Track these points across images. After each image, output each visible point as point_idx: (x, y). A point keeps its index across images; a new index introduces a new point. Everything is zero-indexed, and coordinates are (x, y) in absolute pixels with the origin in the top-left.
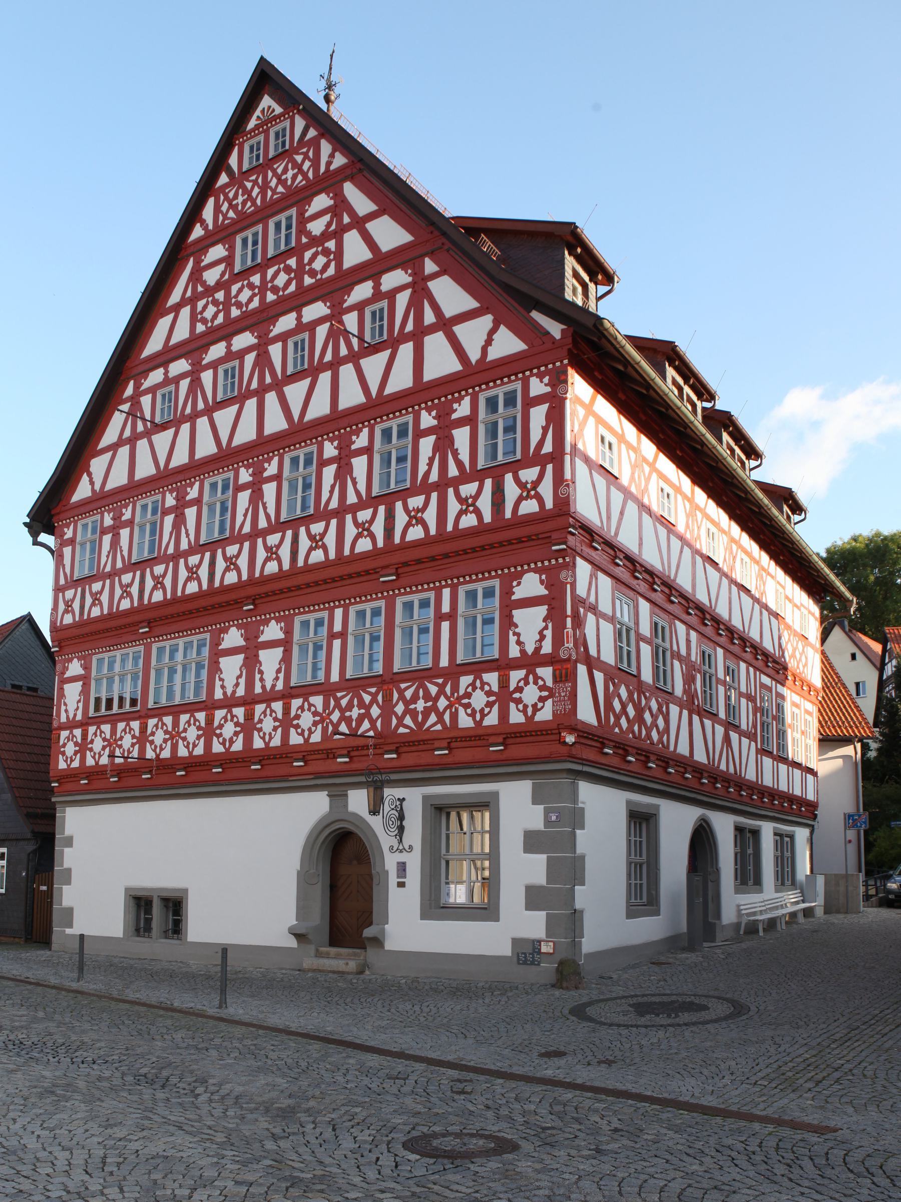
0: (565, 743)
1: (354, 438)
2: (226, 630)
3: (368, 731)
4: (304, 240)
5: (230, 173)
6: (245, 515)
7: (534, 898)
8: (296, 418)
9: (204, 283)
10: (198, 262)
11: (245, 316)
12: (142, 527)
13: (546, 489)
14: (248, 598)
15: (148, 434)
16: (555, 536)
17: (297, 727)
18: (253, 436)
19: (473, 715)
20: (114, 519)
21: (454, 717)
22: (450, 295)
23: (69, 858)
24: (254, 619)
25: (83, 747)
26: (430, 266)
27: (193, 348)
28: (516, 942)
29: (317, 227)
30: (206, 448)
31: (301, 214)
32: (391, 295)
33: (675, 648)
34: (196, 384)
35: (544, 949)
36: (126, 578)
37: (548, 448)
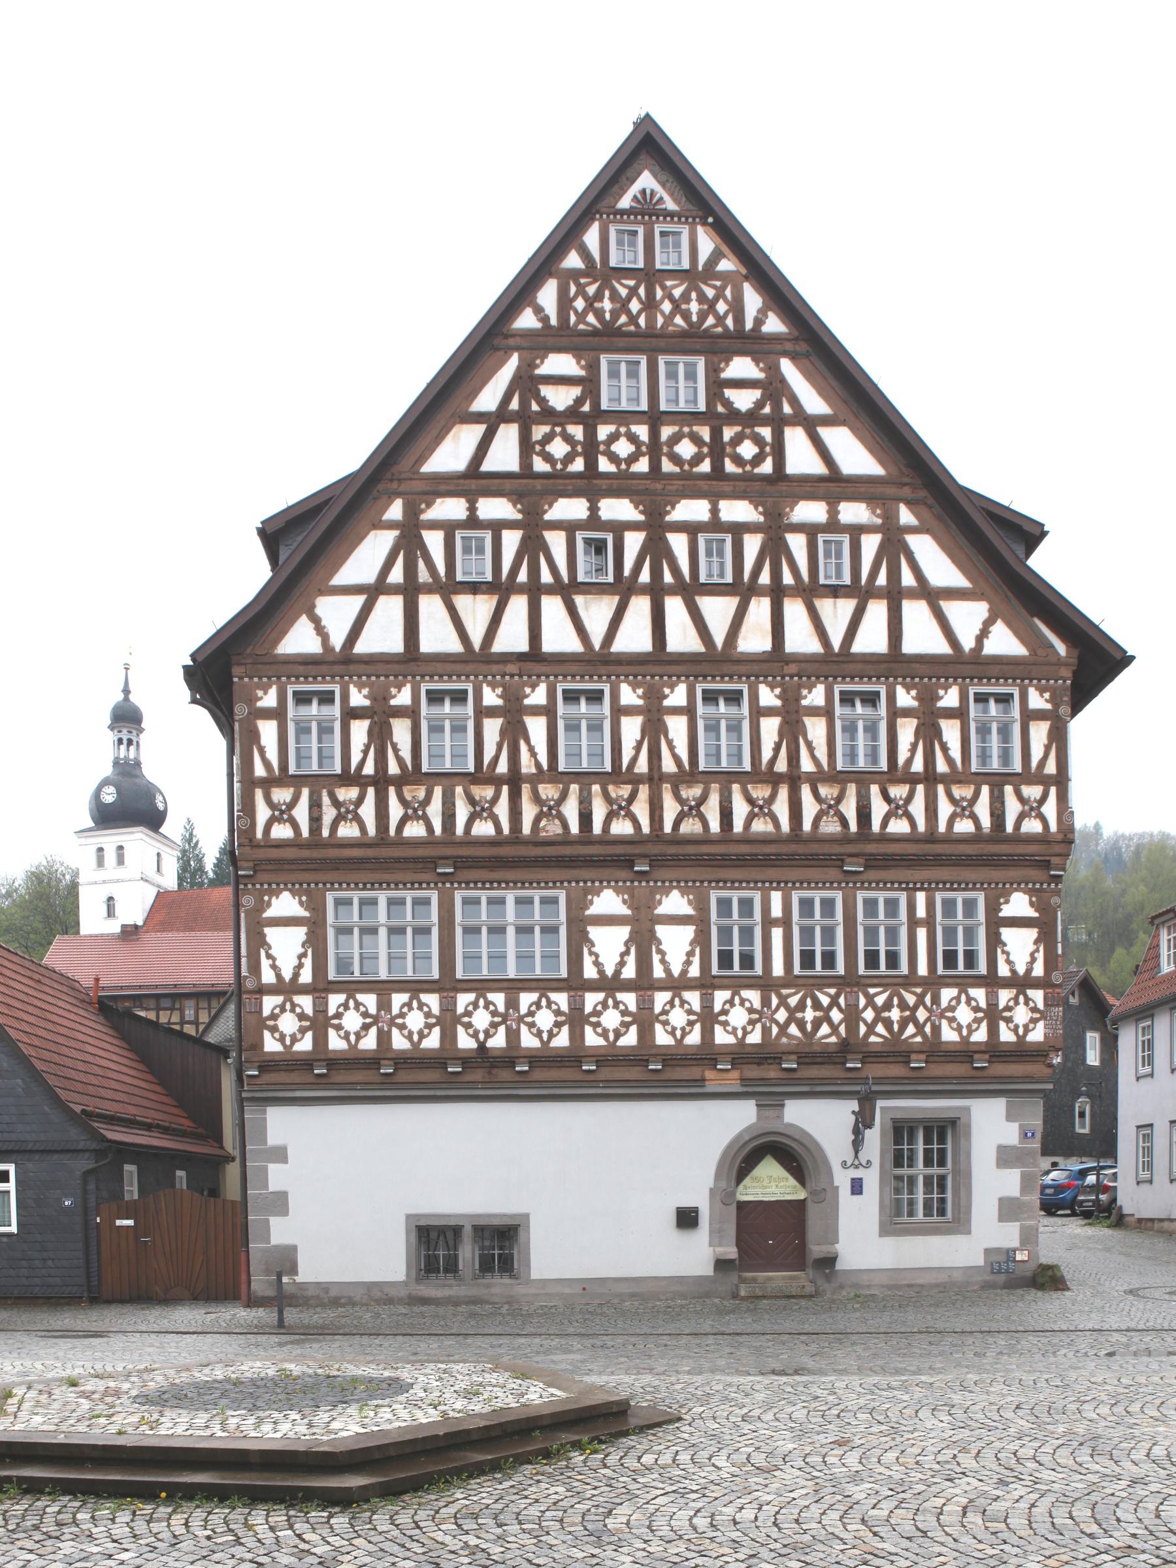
0: (1050, 1066)
1: (805, 692)
4: (535, 407)
13: (1050, 809)
21: (936, 1030)
24: (644, 884)
28: (987, 1251)
35: (1019, 1257)
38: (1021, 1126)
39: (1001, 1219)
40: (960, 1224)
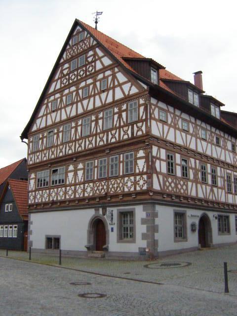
0: (150, 195)
2: (69, 166)
7: (144, 236)
8: (85, 109)
9: (63, 74)
10: (62, 68)
12: (35, 142)
13: (144, 128)
14: (74, 157)
15: (50, 113)
16: (146, 140)
19: (128, 188)
20: (119, 109)
21: (124, 188)
22: (121, 78)
23: (32, 227)
25: (35, 197)
26: (116, 70)
28: (139, 248)
29: (90, 60)
30: (64, 117)
31: (86, 56)
33: (190, 166)
34: (95, 86)
36: (45, 152)
37: (144, 118)
38: (146, 213)
39: (143, 239)
40: (134, 241)
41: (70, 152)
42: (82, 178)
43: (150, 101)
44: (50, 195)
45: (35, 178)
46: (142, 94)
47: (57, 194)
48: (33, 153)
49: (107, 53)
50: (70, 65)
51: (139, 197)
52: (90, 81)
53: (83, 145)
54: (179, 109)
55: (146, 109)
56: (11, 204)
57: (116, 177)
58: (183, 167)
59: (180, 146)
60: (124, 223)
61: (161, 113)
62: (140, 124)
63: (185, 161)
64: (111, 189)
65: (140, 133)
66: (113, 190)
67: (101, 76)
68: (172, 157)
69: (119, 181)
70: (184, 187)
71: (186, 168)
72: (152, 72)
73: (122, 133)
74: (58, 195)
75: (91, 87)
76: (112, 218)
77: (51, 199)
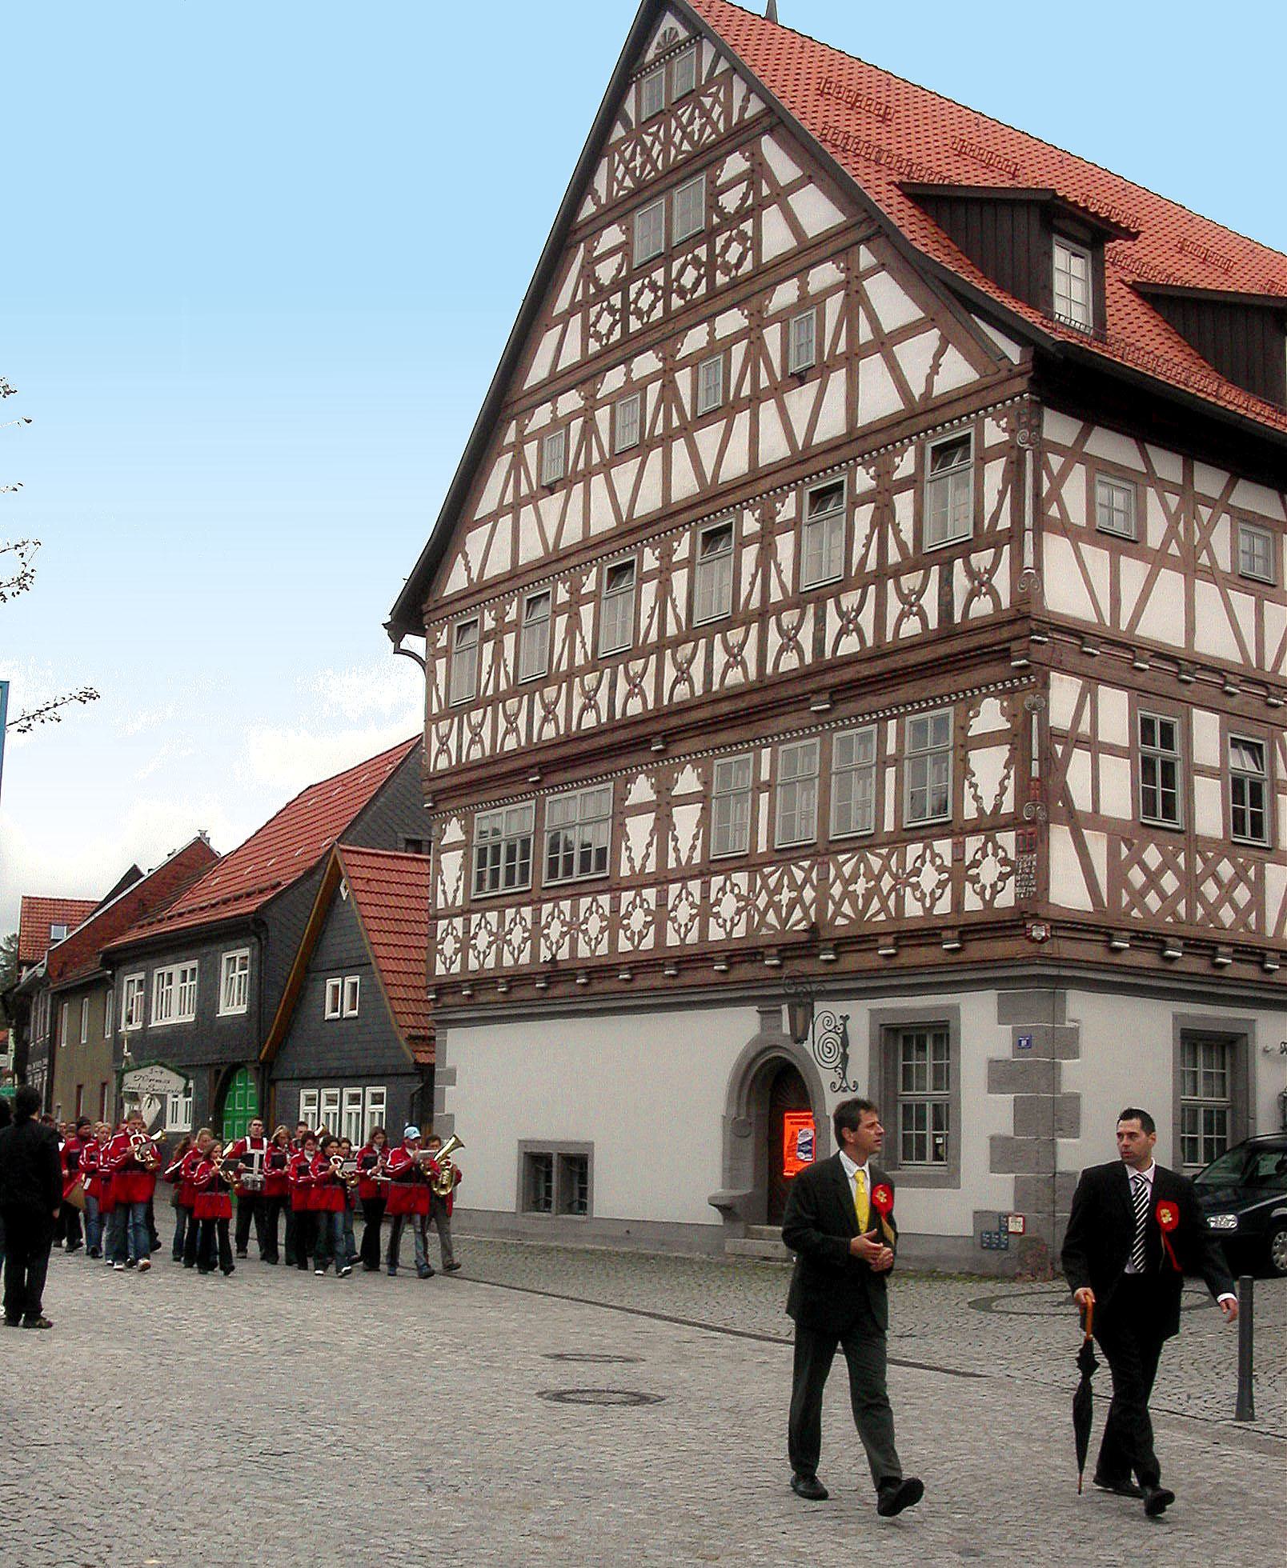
0: (1033, 940)
2: (631, 780)
3: (877, 913)
5: (627, 123)
6: (752, 584)
10: (589, 251)
11: (647, 329)
13: (1002, 581)
14: (656, 734)
15: (533, 499)
17: (717, 915)
18: (745, 468)
20: (877, 477)
21: (900, 900)
22: (891, 301)
23: (452, 1100)
25: (465, 945)
26: (866, 257)
27: (585, 374)
29: (730, 201)
32: (642, 386)
34: (757, 352)
37: (1005, 522)
40: (951, 1180)
41: (635, 707)
42: (693, 847)
43: (1039, 426)
44: (536, 933)
45: (466, 845)
46: (994, 395)
47: (573, 927)
48: (454, 711)
49: (819, 166)
50: (629, 231)
51: (978, 950)
52: (731, 321)
53: (697, 671)
54: (1214, 460)
55: (1014, 478)
56: (357, 979)
57: (862, 844)
58: (1238, 784)
59: (1217, 669)
60: (907, 1086)
61: (1101, 493)
62: (982, 559)
63: (1255, 750)
64: (839, 905)
65: (982, 607)
66: (846, 908)
67: (785, 294)
68: (1167, 729)
69: (876, 863)
70: (1242, 894)
71: (1256, 789)
72: (1060, 257)
73: (894, 606)
74: (578, 931)
75: (739, 351)
76: (845, 1058)
77: (545, 955)
